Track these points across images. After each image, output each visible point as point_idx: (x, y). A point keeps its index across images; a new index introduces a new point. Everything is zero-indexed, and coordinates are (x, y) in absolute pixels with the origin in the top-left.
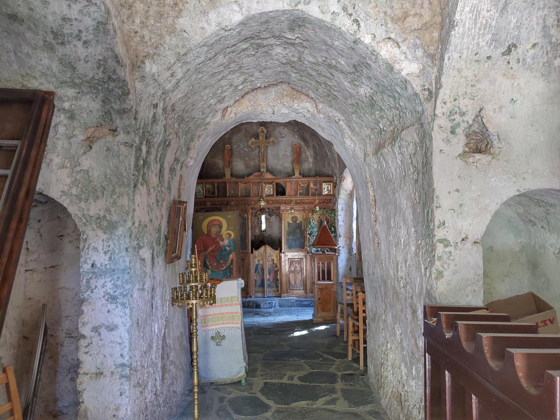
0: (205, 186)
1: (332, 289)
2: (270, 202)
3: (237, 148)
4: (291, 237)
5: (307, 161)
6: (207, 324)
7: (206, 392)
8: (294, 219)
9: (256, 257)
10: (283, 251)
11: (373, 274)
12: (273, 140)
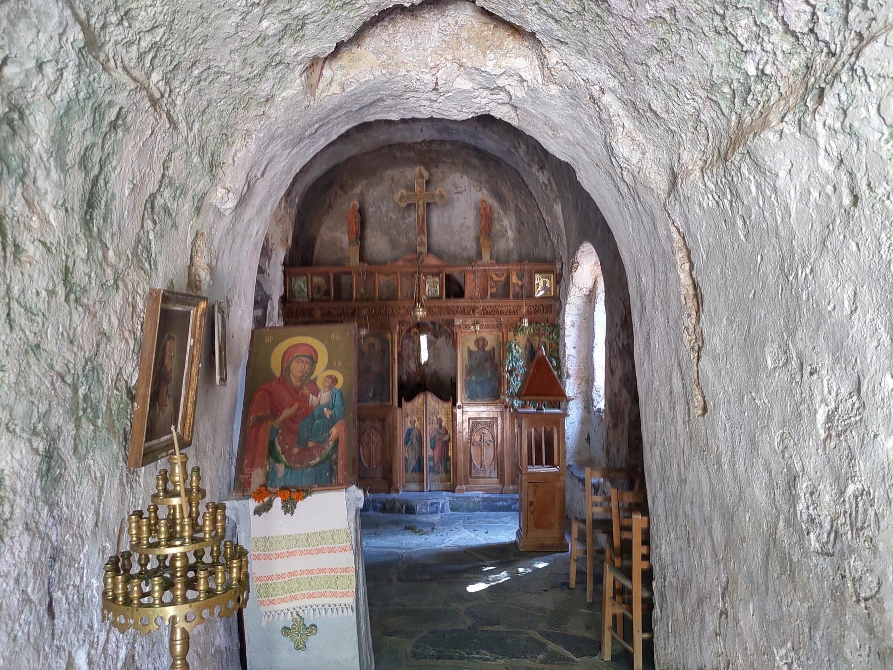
1: (557, 484)
4: (473, 378)
5: (504, 236)
6: (271, 598)
8: (481, 342)
9: (407, 415)
10: (459, 403)
11: (683, 481)
12: (440, 192)
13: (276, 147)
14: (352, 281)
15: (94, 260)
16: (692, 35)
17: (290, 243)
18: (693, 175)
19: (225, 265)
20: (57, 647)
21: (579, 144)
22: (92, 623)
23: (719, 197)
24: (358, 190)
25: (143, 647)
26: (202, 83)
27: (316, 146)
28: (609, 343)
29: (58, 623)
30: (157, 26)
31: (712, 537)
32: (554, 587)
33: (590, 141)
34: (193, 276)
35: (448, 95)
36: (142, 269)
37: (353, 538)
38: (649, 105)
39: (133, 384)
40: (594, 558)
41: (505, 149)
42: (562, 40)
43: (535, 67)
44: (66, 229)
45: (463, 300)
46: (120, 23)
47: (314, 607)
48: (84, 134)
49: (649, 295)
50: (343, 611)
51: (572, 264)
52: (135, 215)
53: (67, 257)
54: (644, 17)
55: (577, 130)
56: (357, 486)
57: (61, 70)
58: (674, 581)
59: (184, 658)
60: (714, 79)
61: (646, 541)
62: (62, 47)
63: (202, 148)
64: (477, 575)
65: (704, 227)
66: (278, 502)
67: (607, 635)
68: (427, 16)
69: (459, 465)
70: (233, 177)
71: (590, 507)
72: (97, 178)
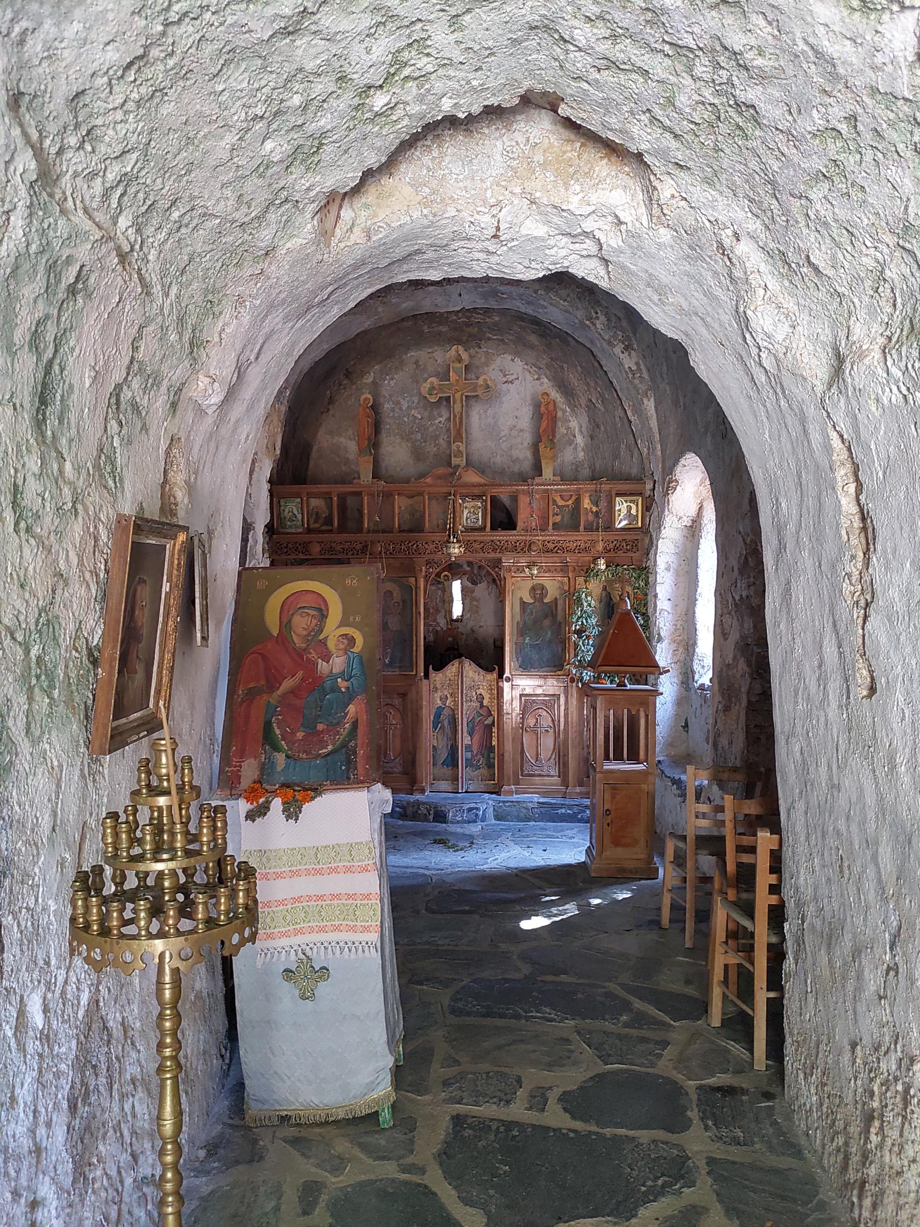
0: (308, 503)
1: (644, 787)
2: (476, 545)
3: (393, 410)
7: (261, 1158)
8: (538, 591)
10: (507, 674)
11: (835, 787)
12: (485, 380)
13: (275, 319)
14: (362, 505)
15: (48, 476)
16: (880, 155)
17: (278, 452)
18: (871, 357)
19: (206, 481)
20: (6, 989)
21: (696, 314)
22: (49, 958)
23: (908, 389)
24: (369, 379)
25: (109, 990)
26: (183, 230)
27: (327, 316)
28: (720, 593)
29: (8, 957)
30: (128, 151)
31: (877, 865)
32: (639, 926)
33: (713, 309)
34: (167, 497)
35: (513, 244)
36: (105, 487)
37: (378, 855)
38: (808, 257)
39: (95, 643)
40: (697, 889)
41: (577, 321)
42: (682, 163)
43: (638, 204)
44: (15, 433)
45: (514, 532)
46: (81, 147)
47: (325, 944)
48: (35, 302)
49: (791, 527)
50: (363, 951)
51: (669, 483)
52: (97, 413)
53: (16, 471)
54: (809, 129)
55: (696, 294)
56: (383, 784)
57: (7, 212)
58: (818, 923)
59: (174, 1007)
60: (911, 219)
61: (776, 866)
62: (8, 181)
63: (181, 320)
64: (534, 907)
65: (882, 432)
66: (277, 804)
67: (717, 992)
68: (486, 131)
69: (506, 757)
70: (219, 361)
71: (693, 819)
72: (50, 363)
